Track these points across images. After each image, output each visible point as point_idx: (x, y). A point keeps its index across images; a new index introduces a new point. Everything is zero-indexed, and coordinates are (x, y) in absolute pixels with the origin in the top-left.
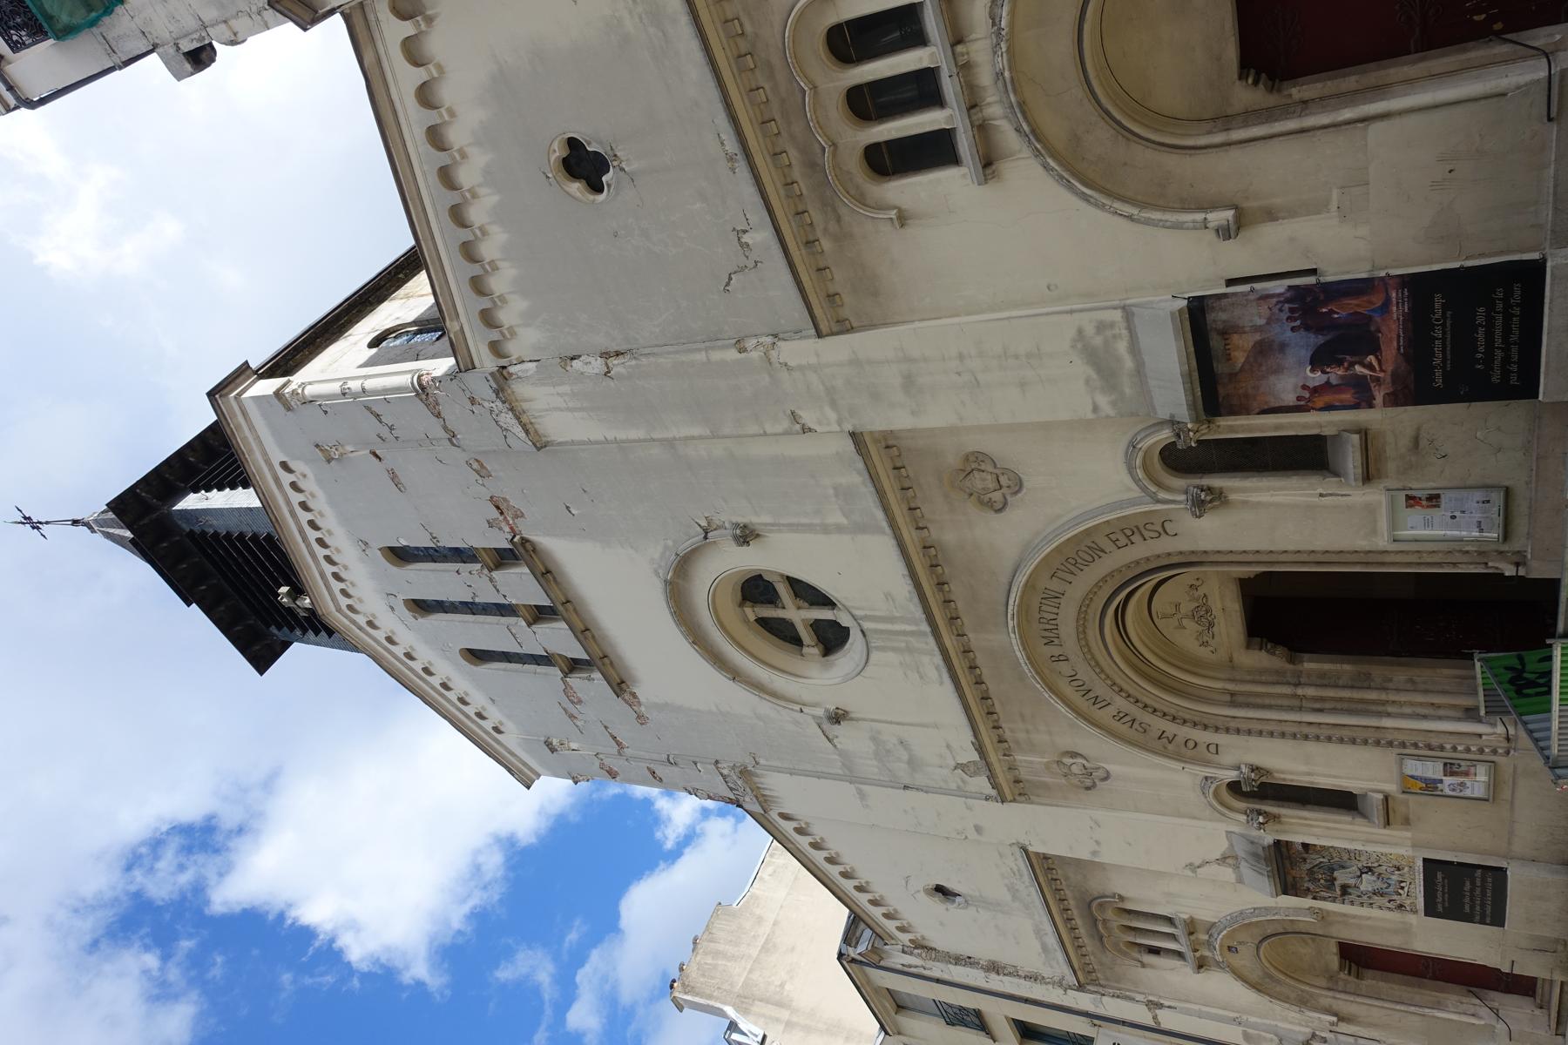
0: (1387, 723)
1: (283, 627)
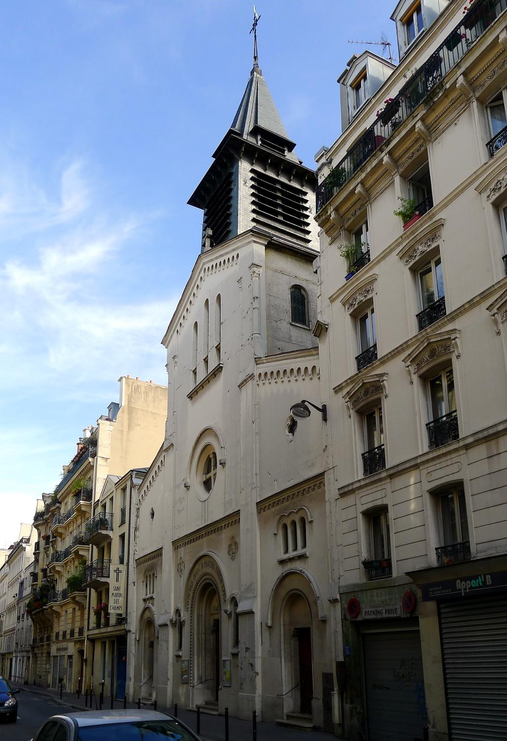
0: (196, 657)
1: (230, 172)
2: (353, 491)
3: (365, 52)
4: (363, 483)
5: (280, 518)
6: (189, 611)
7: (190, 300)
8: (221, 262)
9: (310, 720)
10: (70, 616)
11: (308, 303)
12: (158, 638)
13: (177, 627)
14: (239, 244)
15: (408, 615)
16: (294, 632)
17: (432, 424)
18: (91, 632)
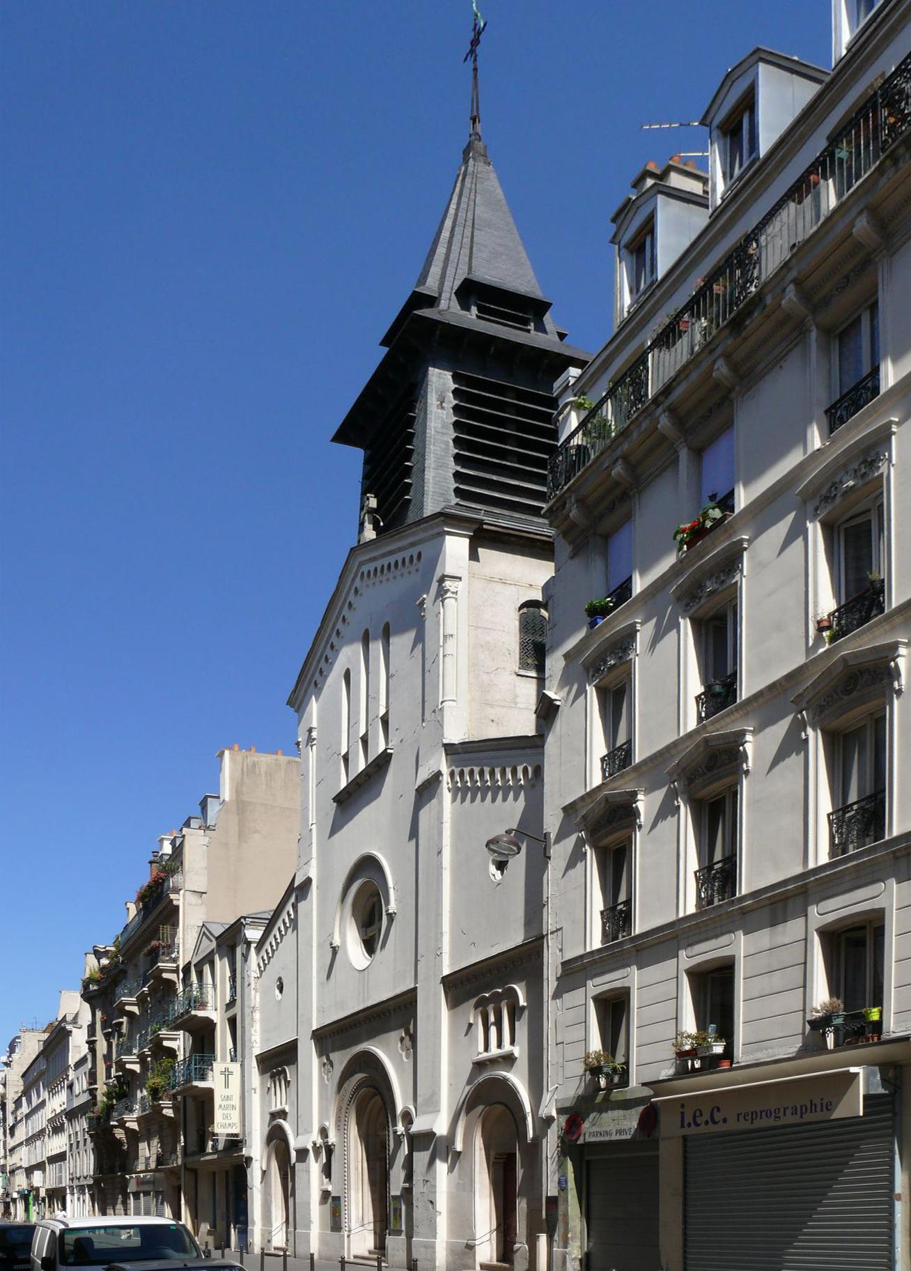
3: (754, 53)
7: (336, 630)
8: (397, 561)
14: (421, 536)
16: (496, 1158)
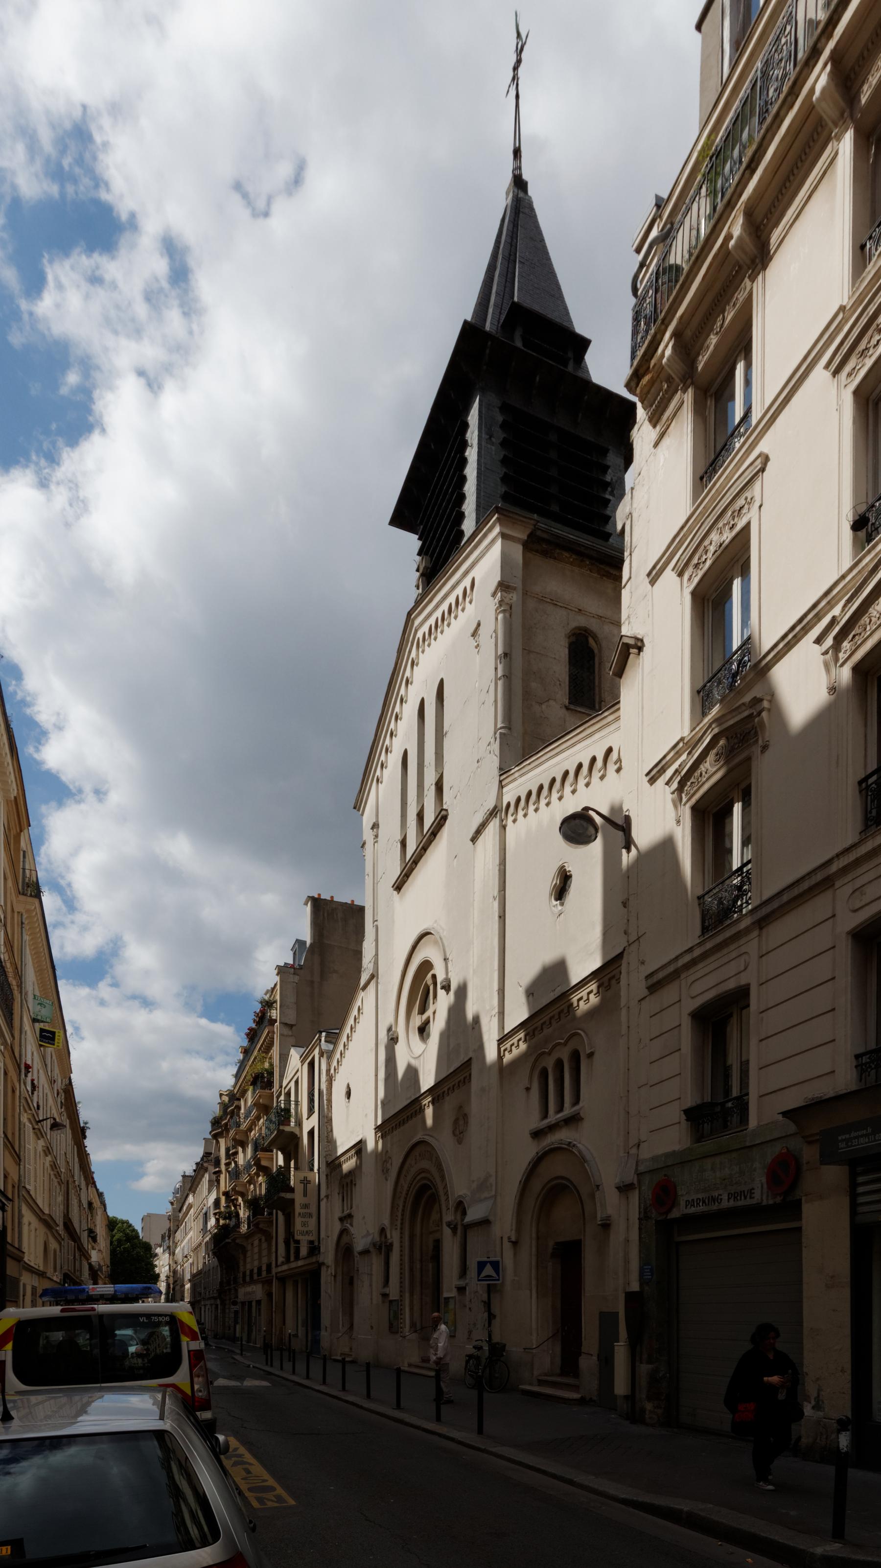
2: (676, 975)
4: (697, 952)
5: (536, 1060)
6: (399, 1229)
9: (575, 1388)
10: (256, 1250)
11: (600, 664)
12: (358, 1270)
13: (383, 1253)
15: (779, 1200)
17: (874, 778)
18: (280, 1269)
